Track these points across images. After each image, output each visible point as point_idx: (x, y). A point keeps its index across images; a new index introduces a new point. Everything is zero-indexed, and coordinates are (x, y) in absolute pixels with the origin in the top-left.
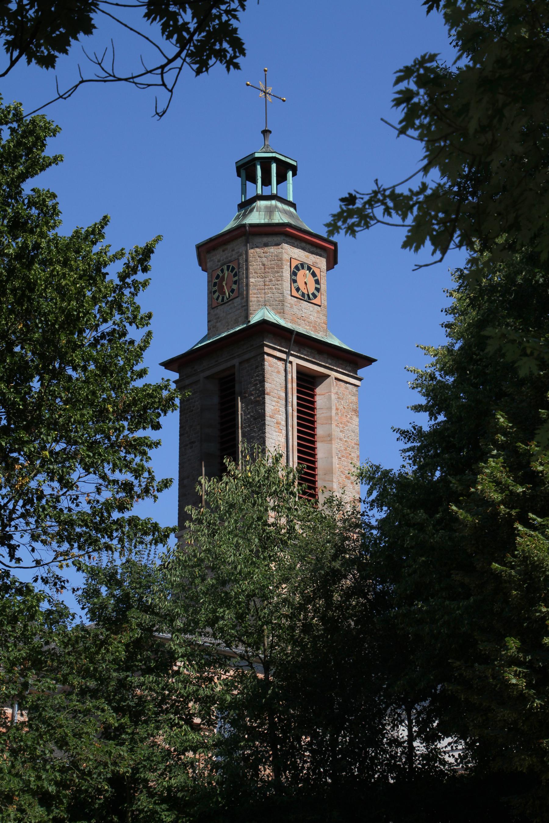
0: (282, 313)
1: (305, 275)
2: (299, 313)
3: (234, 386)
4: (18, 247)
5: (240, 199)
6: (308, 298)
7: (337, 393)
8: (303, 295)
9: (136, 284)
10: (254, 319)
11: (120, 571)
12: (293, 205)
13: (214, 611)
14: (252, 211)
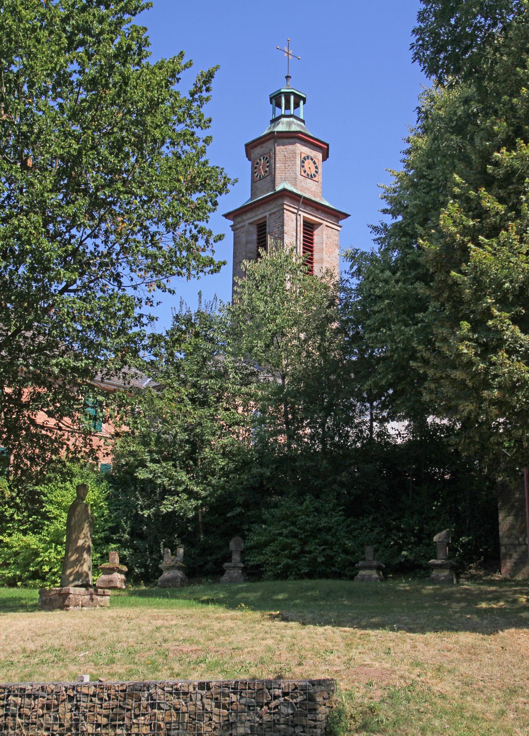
0: (295, 185)
1: (309, 163)
2: (305, 186)
3: (265, 229)
4: (117, 48)
5: (272, 117)
6: (311, 177)
7: (326, 234)
8: (308, 175)
9: (201, 99)
10: (278, 188)
11: (193, 317)
12: (303, 121)
13: (251, 342)
14: (278, 124)
